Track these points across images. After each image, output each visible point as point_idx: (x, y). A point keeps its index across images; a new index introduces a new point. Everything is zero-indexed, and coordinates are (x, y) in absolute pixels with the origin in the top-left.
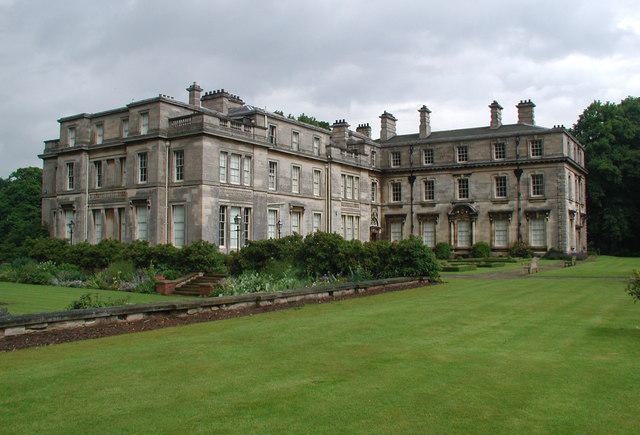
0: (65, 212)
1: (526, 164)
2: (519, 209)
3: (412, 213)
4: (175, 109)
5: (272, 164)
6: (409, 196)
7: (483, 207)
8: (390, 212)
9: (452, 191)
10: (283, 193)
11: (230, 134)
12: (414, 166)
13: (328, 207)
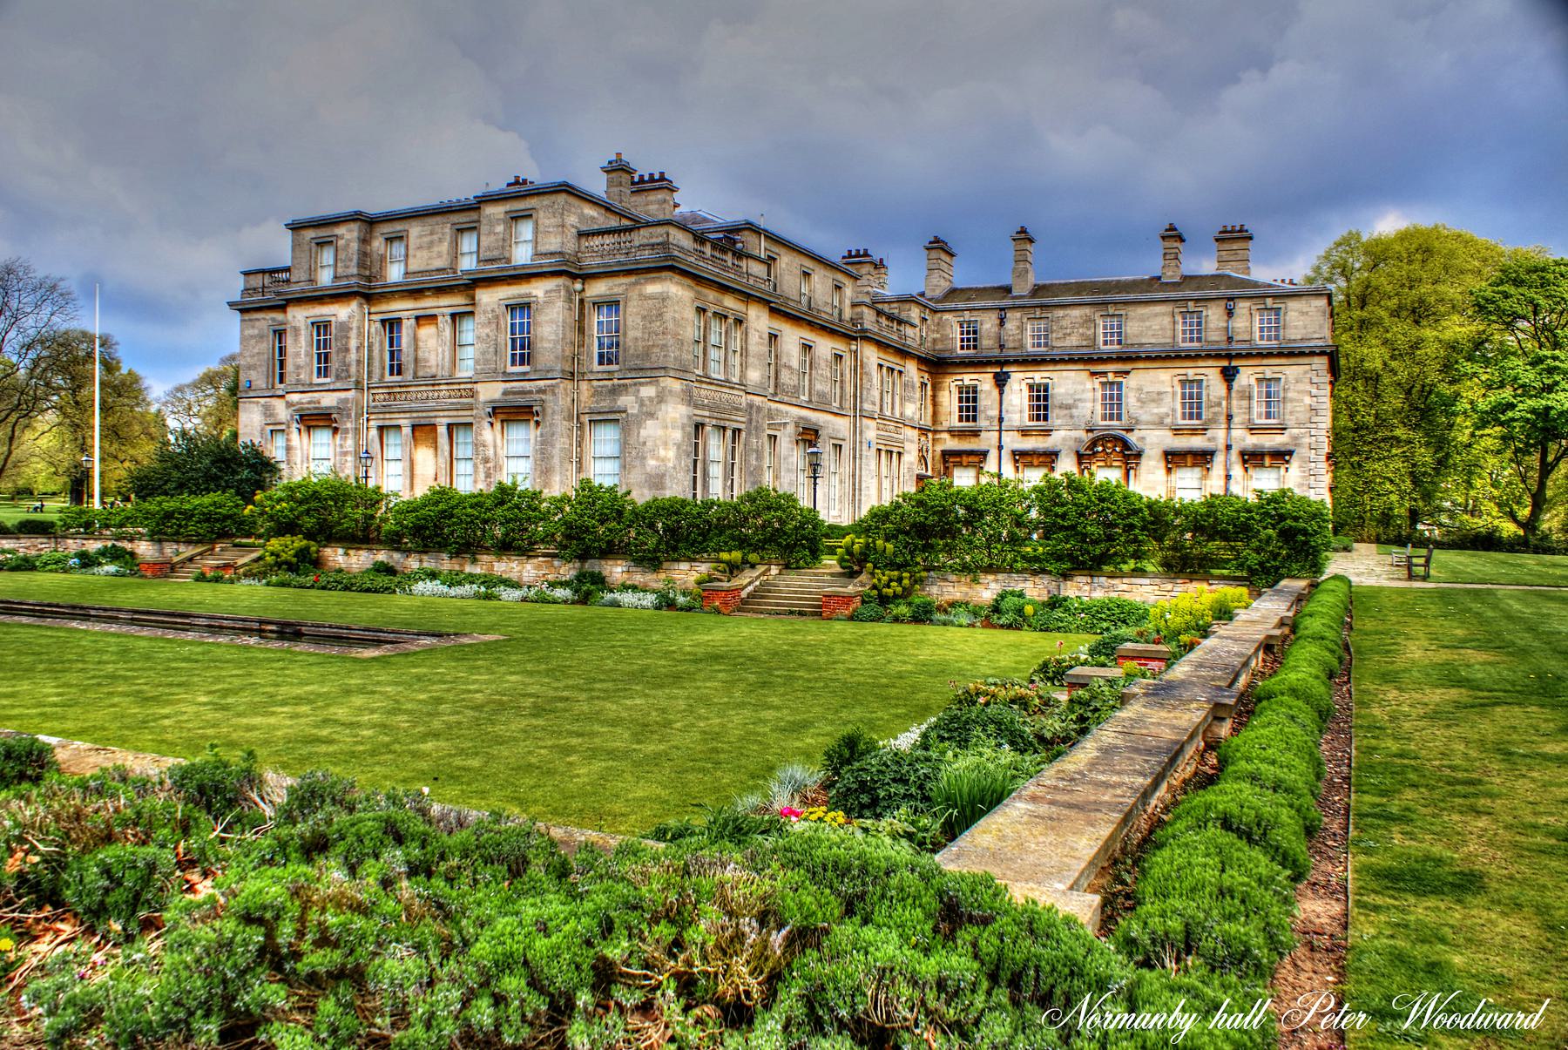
0: (309, 428)
1: (1249, 356)
2: (1228, 447)
3: (1000, 448)
4: (590, 211)
5: (773, 337)
6: (995, 413)
7: (1153, 441)
8: (952, 444)
9: (1089, 405)
10: (786, 399)
11: (709, 269)
12: (1235, 346)
13: (856, 430)
